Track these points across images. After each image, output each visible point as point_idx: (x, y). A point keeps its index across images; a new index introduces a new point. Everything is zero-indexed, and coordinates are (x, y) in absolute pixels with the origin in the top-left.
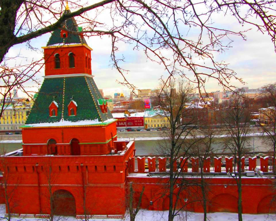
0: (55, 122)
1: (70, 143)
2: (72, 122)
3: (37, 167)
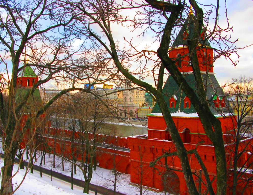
0: (173, 112)
1: (183, 131)
2: (186, 113)
3: (153, 148)
